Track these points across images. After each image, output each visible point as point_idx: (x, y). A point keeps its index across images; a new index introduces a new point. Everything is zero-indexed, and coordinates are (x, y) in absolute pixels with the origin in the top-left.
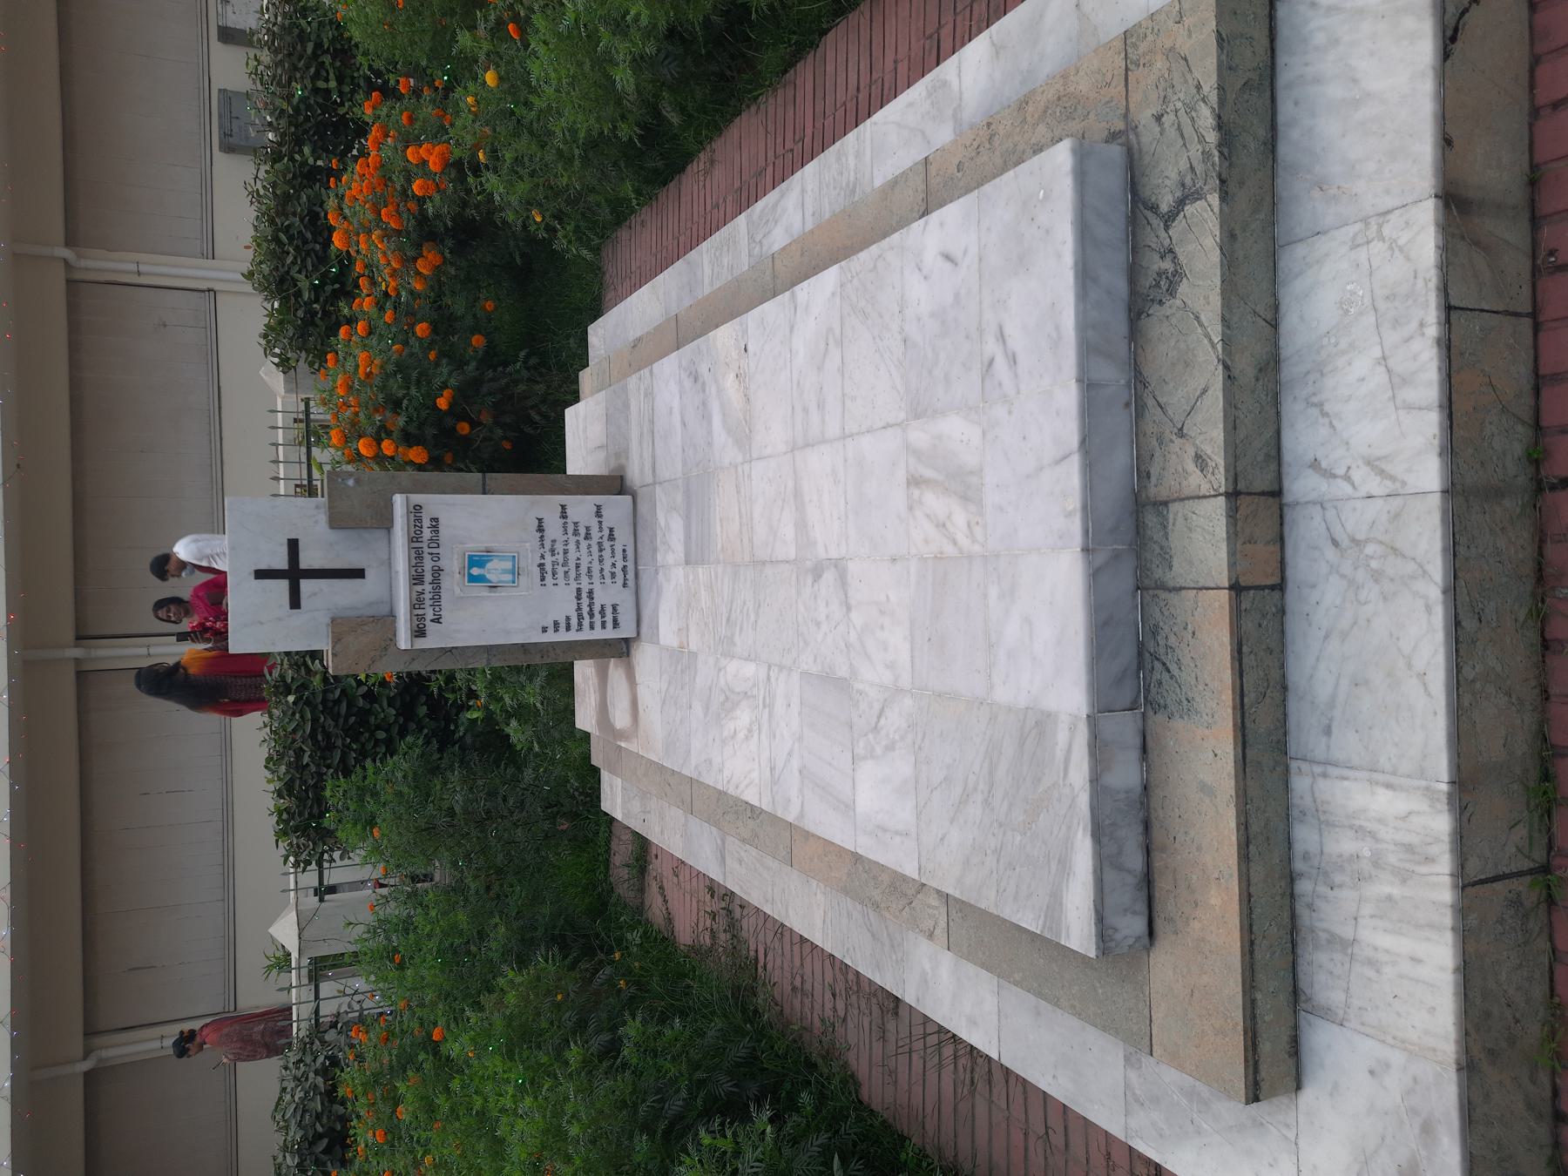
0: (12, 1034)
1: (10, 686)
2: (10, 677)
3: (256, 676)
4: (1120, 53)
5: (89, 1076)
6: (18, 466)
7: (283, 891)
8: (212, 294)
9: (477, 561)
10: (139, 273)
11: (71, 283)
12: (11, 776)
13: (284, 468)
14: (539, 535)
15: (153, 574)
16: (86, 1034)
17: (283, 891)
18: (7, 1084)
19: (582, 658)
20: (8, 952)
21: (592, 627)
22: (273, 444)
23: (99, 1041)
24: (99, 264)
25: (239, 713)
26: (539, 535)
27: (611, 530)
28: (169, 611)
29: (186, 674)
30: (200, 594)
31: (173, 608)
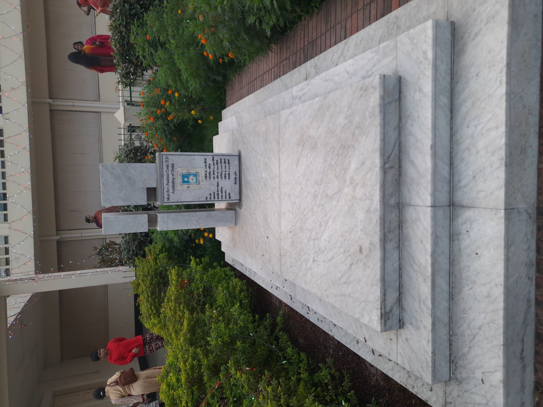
0: (33, 217)
1: (28, 102)
2: (28, 99)
3: (108, 56)
4: (396, 237)
5: (59, 243)
6: (27, 26)
7: (119, 128)
8: (99, 114)
9: (184, 176)
10: (74, 106)
11: (51, 111)
12: (29, 132)
13: (122, 144)
14: (205, 164)
15: (73, 62)
16: (57, 230)
17: (119, 128)
18: (32, 233)
19: (219, 226)
20: (31, 190)
21: (221, 160)
22: (119, 134)
23: (60, 232)
24: (67, 235)
25: (102, 71)
26: (205, 164)
27: (229, 194)
28: (78, 46)
29: (85, 53)
30: (89, 42)
31: (80, 44)
